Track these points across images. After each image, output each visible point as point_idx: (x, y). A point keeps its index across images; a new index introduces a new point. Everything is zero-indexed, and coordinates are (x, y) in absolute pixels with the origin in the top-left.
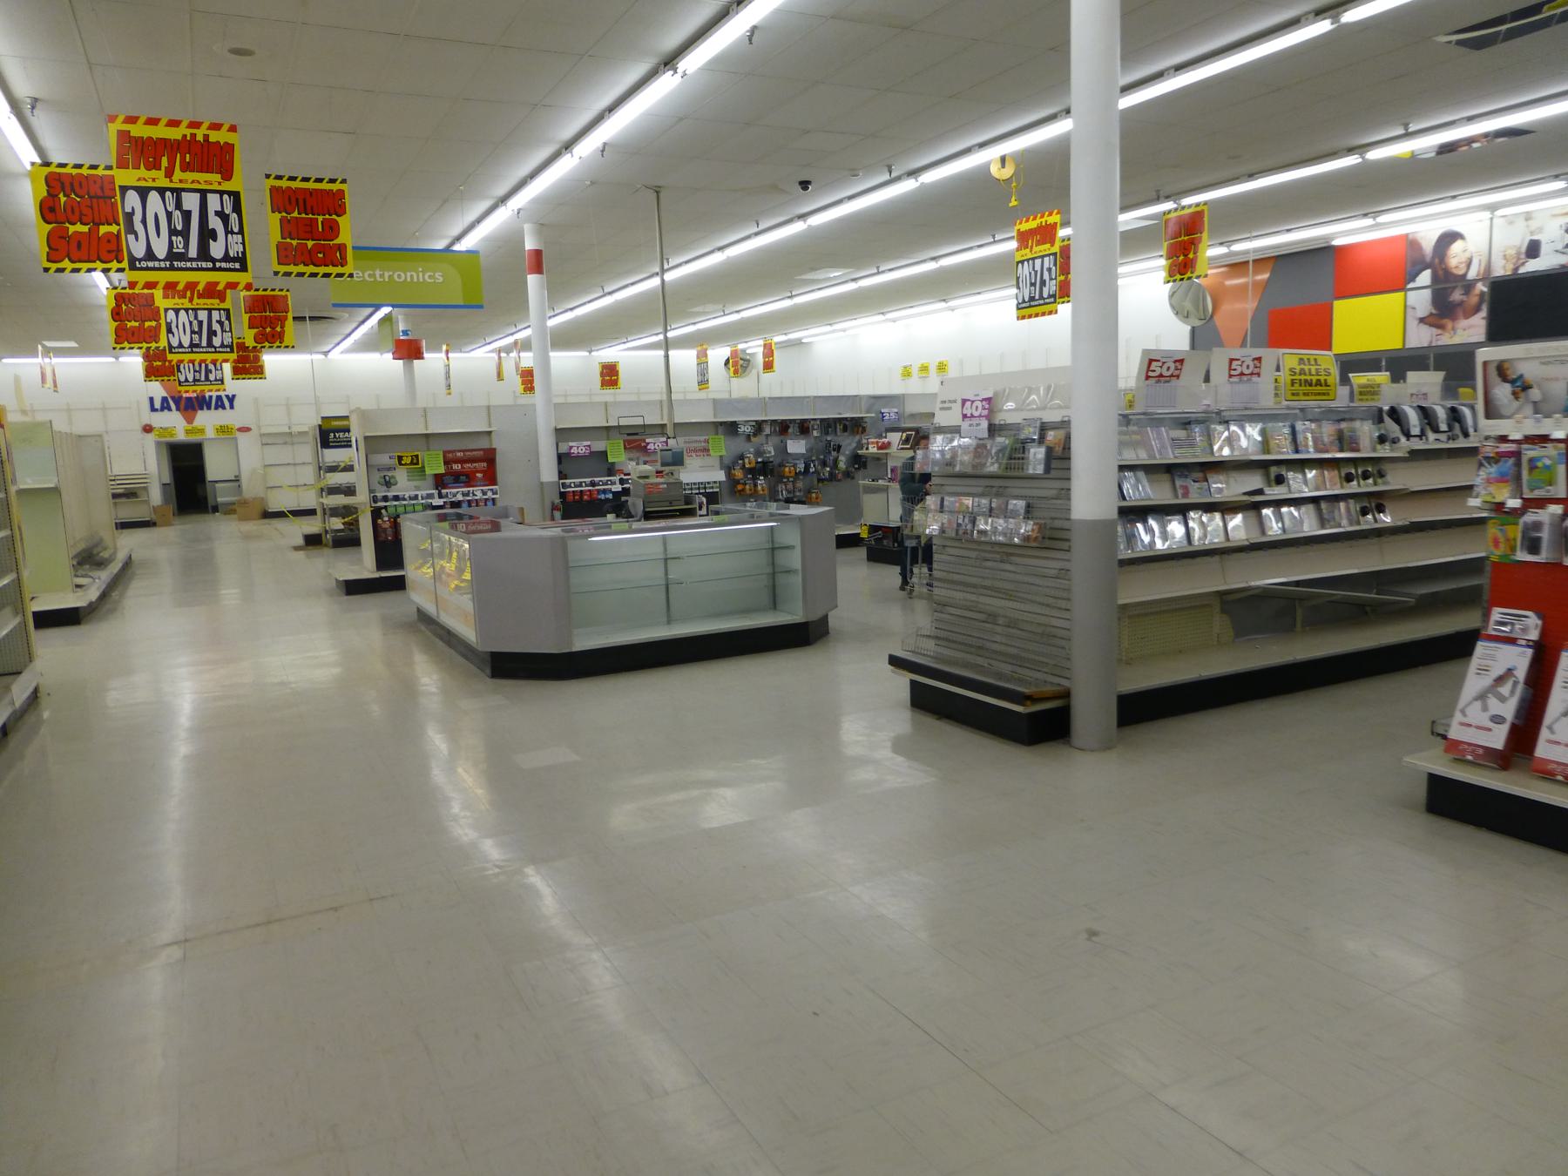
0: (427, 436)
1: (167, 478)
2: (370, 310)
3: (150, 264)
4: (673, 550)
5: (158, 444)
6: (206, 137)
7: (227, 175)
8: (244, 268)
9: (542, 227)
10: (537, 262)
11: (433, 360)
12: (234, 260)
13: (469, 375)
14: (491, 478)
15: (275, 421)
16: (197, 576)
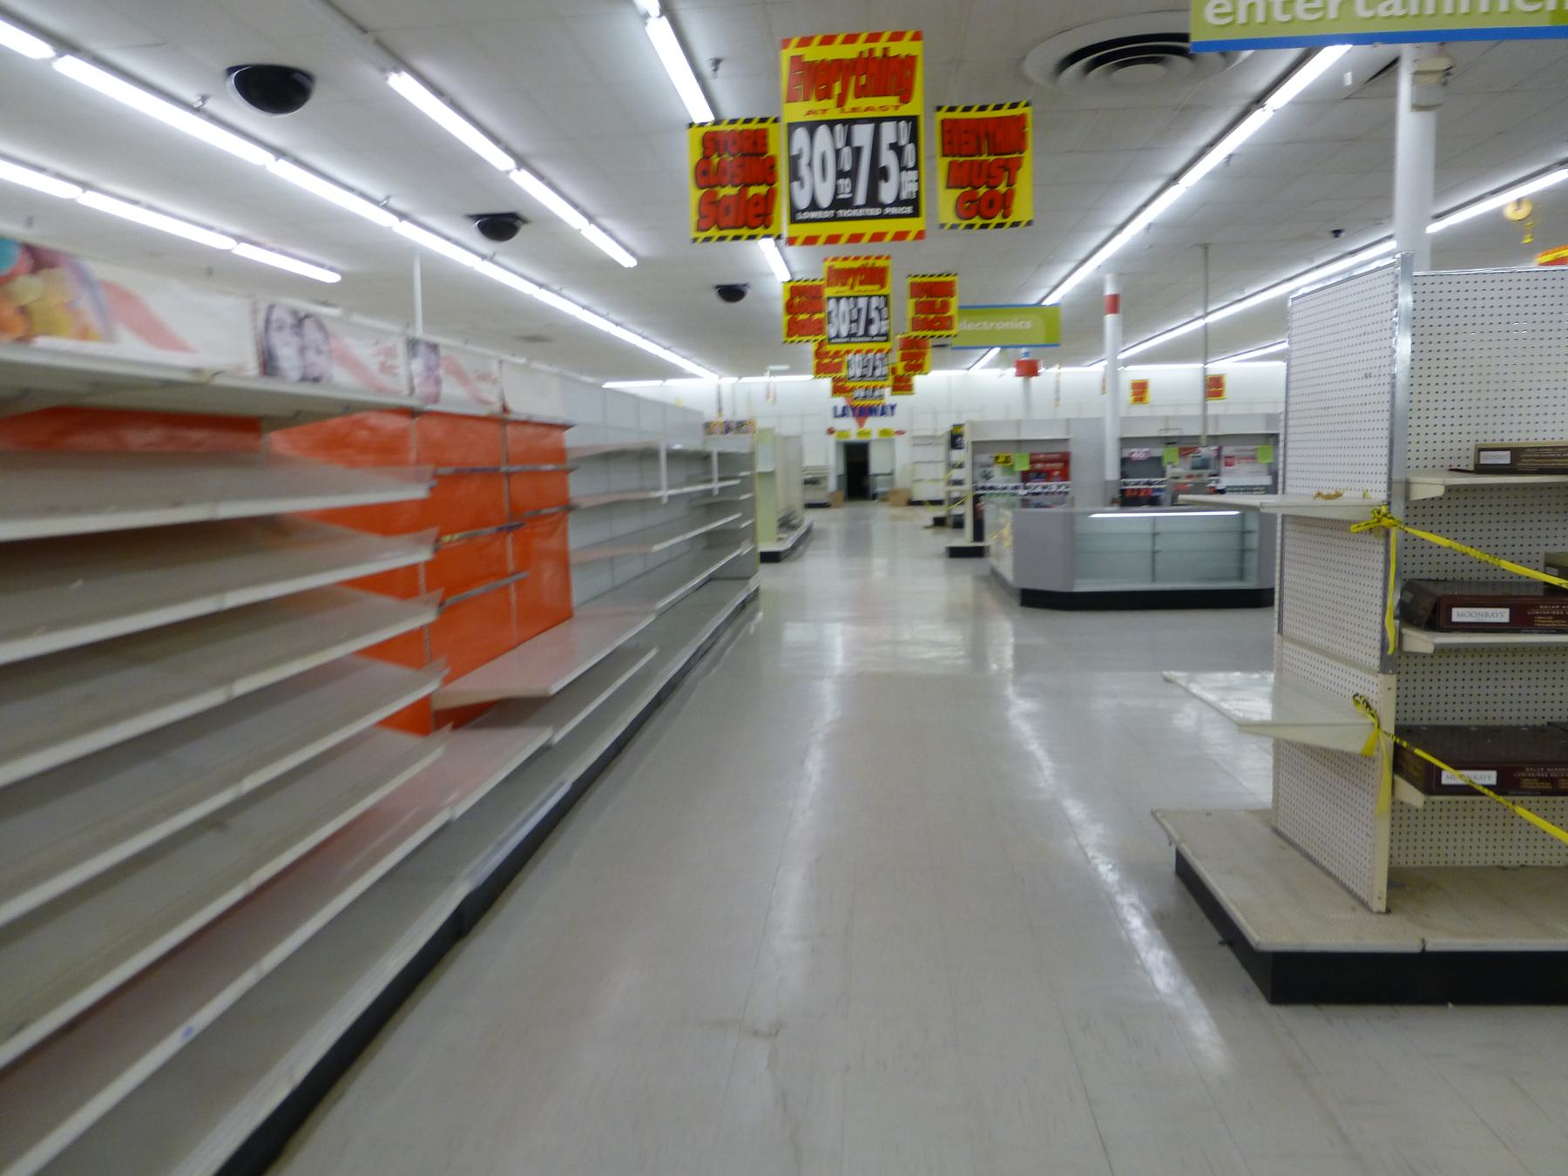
0: (1019, 442)
1: (841, 470)
2: (1292, 54)
3: (813, 215)
4: (1160, 528)
5: (838, 443)
6: (886, 50)
7: (883, 285)
8: (916, 214)
9: (1120, 276)
10: (1114, 304)
11: (1049, 374)
12: (906, 203)
13: (1078, 392)
14: (1065, 475)
15: (924, 427)
16: (857, 543)
